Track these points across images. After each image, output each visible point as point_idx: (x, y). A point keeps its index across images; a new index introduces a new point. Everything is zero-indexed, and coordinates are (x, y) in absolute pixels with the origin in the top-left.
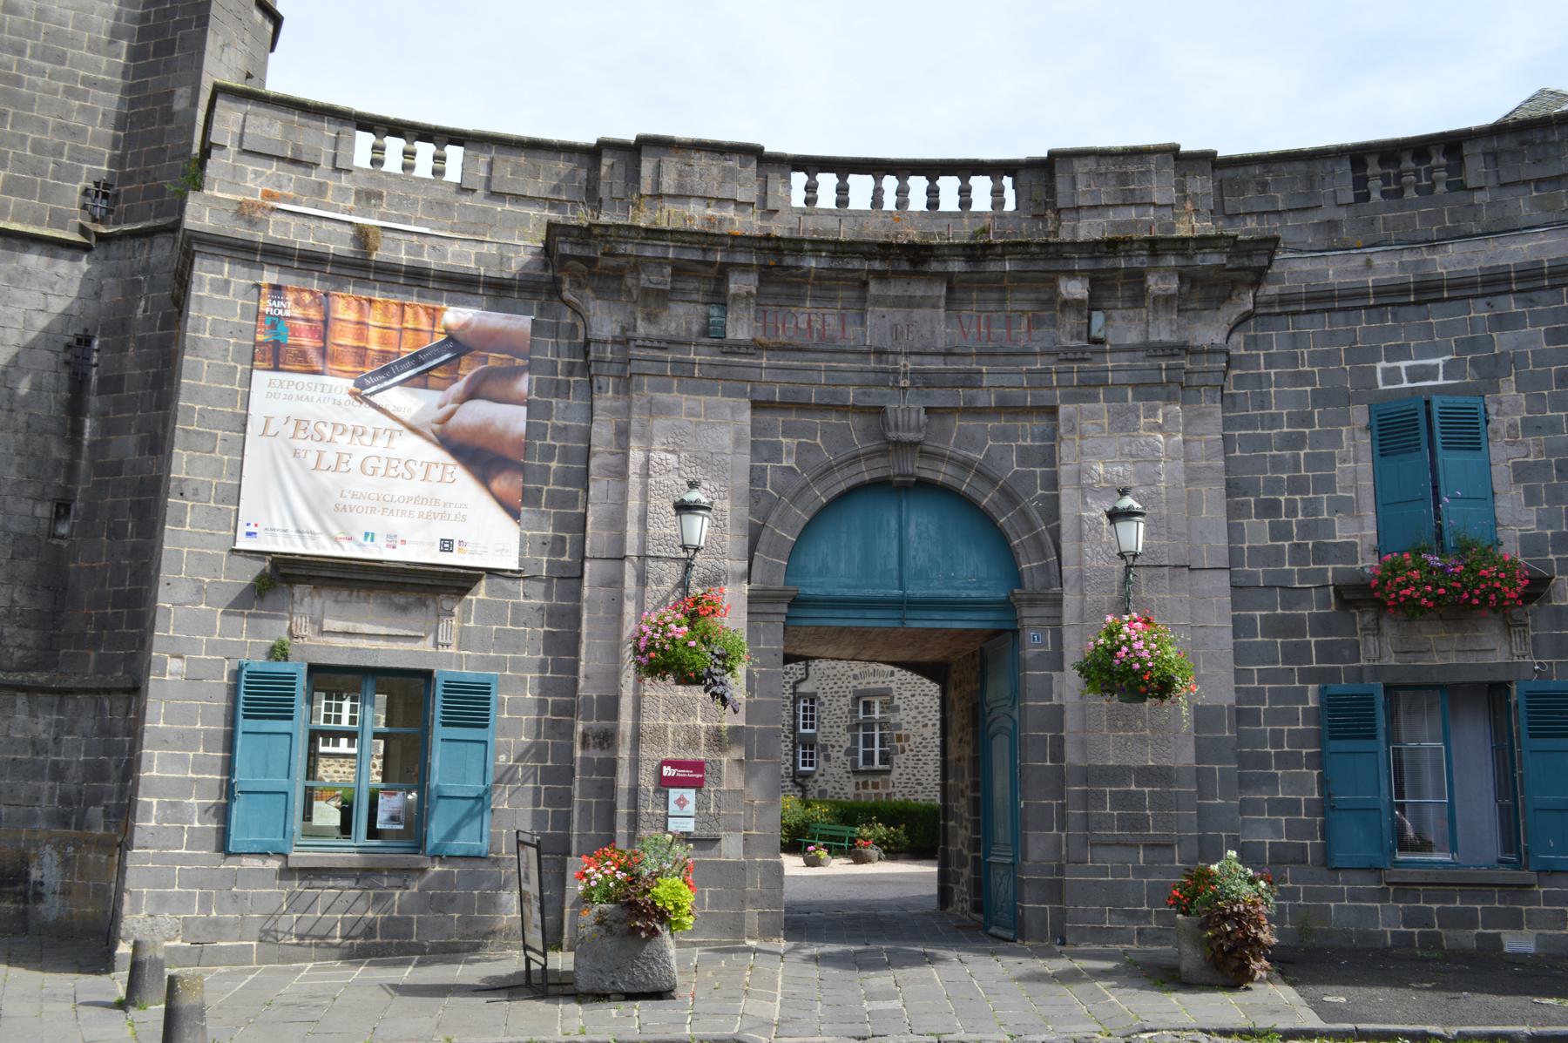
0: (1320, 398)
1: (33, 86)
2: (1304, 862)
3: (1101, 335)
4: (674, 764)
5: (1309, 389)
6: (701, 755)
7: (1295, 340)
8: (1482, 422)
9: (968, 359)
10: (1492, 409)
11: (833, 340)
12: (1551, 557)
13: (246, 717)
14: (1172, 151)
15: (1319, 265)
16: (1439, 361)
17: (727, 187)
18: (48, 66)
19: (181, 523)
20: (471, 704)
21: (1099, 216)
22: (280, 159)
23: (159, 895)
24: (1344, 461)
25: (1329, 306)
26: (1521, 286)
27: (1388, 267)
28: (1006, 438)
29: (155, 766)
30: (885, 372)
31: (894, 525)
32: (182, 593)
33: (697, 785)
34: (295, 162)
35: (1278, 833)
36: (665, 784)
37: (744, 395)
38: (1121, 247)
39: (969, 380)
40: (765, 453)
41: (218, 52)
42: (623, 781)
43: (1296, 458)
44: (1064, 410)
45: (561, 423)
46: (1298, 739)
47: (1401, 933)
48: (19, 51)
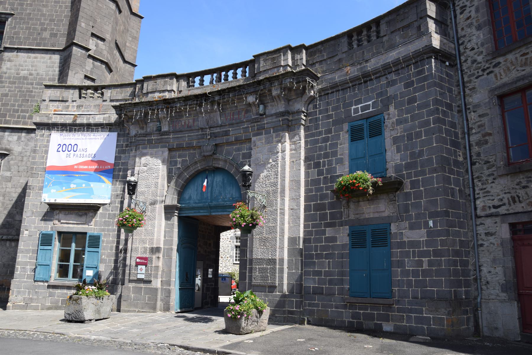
0: (335, 123)
1: (35, 92)
2: (323, 294)
6: (147, 255)
7: (328, 104)
8: (382, 122)
9: (226, 127)
10: (386, 117)
11: (191, 127)
12: (404, 172)
14: (289, 47)
15: (333, 76)
17: (165, 87)
18: (39, 87)
19: (29, 196)
20: (95, 241)
21: (266, 73)
22: (59, 101)
23: (18, 291)
24: (341, 145)
27: (351, 71)
29: (20, 258)
32: (29, 214)
33: (146, 265)
34: (62, 101)
35: (315, 283)
36: (137, 264)
37: (166, 147)
39: (227, 133)
40: (173, 164)
41: (73, 75)
43: (326, 146)
44: (253, 139)
47: (351, 322)
48: (32, 84)
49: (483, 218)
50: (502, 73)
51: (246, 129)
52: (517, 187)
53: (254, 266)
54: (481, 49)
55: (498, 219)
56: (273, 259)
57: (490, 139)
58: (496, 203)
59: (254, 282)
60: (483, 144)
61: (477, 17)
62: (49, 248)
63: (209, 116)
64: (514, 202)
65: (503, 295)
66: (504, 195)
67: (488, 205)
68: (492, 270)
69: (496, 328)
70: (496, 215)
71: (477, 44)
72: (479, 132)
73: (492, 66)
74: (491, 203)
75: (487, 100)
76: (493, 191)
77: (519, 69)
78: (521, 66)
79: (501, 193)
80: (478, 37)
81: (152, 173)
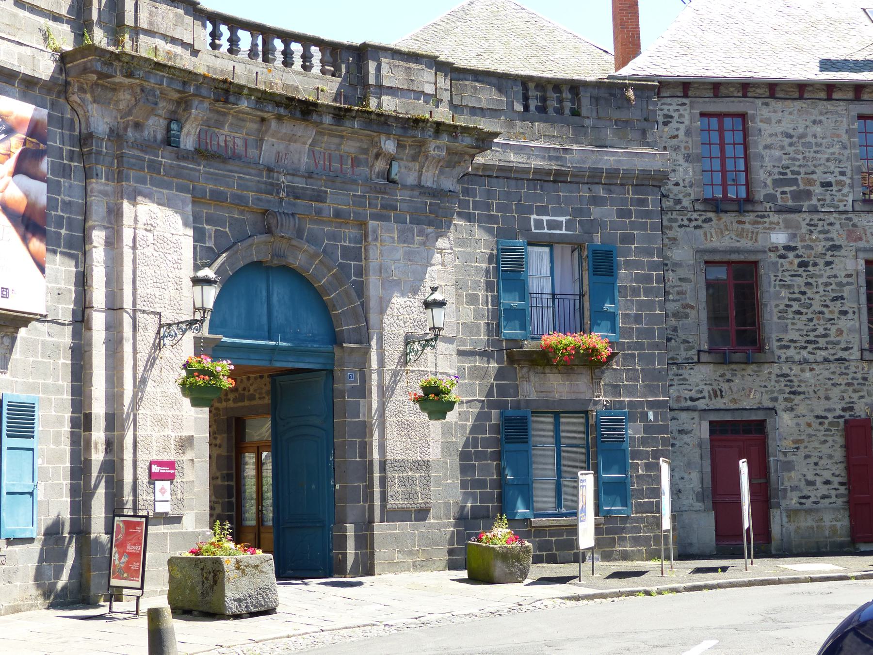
3: (397, 178)
4: (160, 464)
5: (495, 226)
6: (170, 456)
7: (489, 194)
13: (9, 436)
16: (563, 219)
25: (508, 175)
26: (607, 181)
28: (335, 239)
30: (272, 184)
31: (264, 293)
33: (171, 478)
36: (153, 478)
38: (421, 124)
42: (128, 478)
45: (67, 199)
46: (486, 443)
49: (676, 412)
50: (714, 235)
51: (359, 201)
52: (720, 379)
53: (389, 475)
54: (689, 190)
55: (696, 415)
56: (424, 462)
57: (692, 313)
58: (693, 394)
59: (391, 503)
60: (682, 317)
61: (687, 142)
62: (521, 446)
63: (287, 147)
64: (716, 396)
65: (699, 505)
66: (704, 387)
67: (683, 396)
68: (686, 476)
69: (691, 544)
70: (694, 409)
71: (684, 180)
72: (678, 301)
73: (701, 219)
74: (687, 394)
75: (692, 262)
76: (691, 380)
77: (734, 237)
78: (737, 236)
79: (700, 384)
80: (686, 172)
81: (160, 252)
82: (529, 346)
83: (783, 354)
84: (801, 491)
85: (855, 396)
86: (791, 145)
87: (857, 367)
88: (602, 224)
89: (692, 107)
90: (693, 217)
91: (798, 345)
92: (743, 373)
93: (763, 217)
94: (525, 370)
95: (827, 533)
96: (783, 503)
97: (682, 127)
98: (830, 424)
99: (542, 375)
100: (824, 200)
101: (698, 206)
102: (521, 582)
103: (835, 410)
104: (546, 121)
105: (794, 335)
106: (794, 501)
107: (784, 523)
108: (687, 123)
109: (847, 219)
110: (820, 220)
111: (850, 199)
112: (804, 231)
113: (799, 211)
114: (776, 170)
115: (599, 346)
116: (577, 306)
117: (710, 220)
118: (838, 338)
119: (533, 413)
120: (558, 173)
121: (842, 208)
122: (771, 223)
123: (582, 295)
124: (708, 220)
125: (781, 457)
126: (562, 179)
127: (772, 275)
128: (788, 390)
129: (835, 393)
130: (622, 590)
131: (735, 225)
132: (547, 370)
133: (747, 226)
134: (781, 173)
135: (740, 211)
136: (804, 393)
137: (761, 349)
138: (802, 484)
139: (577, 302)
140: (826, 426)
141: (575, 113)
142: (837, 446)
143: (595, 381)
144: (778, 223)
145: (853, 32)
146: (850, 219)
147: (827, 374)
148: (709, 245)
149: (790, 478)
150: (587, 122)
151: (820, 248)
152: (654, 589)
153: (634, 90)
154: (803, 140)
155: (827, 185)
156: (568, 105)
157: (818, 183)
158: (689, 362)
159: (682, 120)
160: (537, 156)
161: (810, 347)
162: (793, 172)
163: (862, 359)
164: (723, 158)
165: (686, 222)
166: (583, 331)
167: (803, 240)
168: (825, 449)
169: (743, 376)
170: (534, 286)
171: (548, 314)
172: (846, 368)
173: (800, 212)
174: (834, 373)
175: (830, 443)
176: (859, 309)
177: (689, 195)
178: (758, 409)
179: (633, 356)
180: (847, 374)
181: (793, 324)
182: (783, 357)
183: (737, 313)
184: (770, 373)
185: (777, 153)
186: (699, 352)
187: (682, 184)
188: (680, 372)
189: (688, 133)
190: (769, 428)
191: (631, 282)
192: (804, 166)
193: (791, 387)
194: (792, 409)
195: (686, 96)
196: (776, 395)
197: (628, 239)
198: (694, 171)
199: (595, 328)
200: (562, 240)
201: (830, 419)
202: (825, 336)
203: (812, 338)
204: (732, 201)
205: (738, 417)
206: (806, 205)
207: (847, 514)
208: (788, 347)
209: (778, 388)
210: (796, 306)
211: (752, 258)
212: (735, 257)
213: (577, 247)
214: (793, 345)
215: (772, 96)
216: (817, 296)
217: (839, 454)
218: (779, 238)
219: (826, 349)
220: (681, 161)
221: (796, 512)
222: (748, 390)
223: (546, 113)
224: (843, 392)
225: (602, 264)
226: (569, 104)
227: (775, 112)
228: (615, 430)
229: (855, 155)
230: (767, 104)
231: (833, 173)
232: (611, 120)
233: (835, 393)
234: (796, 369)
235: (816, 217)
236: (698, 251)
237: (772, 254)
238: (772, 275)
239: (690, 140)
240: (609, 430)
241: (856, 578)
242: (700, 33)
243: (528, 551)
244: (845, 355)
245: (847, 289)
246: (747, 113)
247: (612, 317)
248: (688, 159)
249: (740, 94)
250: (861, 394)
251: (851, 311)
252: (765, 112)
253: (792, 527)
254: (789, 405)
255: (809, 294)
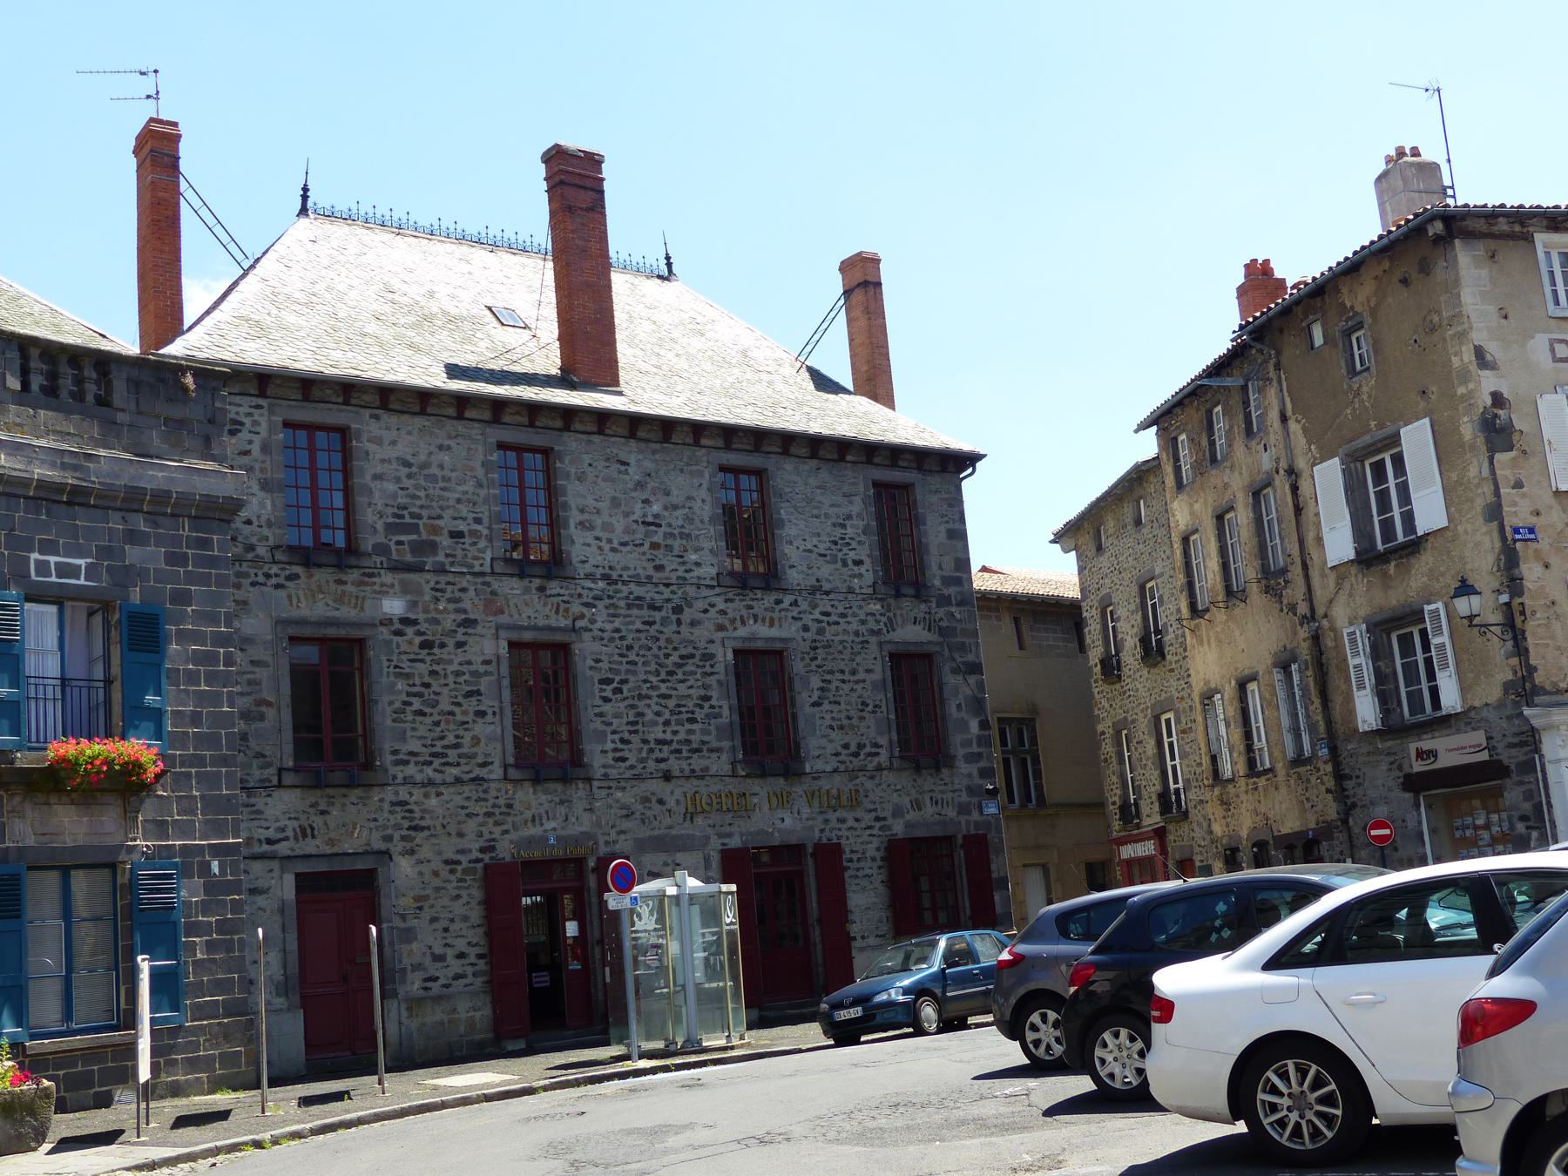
16: (82, 562)
54: (265, 531)
55: (275, 865)
57: (270, 713)
58: (271, 834)
64: (305, 836)
67: (256, 836)
74: (262, 834)
76: (270, 812)
80: (262, 505)
82: (23, 760)
83: (400, 772)
84: (425, 970)
85: (497, 830)
86: (409, 476)
87: (499, 790)
88: (142, 574)
89: (271, 412)
90: (272, 572)
91: (421, 759)
92: (343, 800)
93: (372, 575)
94: (17, 800)
95: (462, 1029)
96: (401, 991)
97: (257, 440)
98: (464, 871)
99: (45, 808)
100: (453, 556)
101: (279, 556)
102: (34, 1149)
103: (470, 851)
104: (57, 410)
105: (414, 745)
106: (416, 986)
107: (403, 1020)
108: (264, 434)
109: (484, 584)
110: (449, 583)
111: (488, 556)
112: (427, 598)
113: (418, 569)
114: (390, 511)
115: (143, 760)
116: (101, 697)
117: (296, 577)
118: (474, 750)
119: (30, 868)
120: (75, 490)
121: (477, 569)
122: (382, 585)
123: (108, 682)
124: (293, 577)
125: (398, 922)
126: (81, 500)
127: (384, 658)
128: (406, 824)
129: (471, 826)
130: (219, 1144)
131: (333, 586)
132: (53, 799)
133: (350, 588)
134: (395, 515)
135: (340, 566)
136: (428, 828)
137: (368, 765)
138: (428, 960)
139: (101, 692)
140: (459, 875)
141: (103, 402)
142: (474, 903)
143: (129, 815)
144: (393, 586)
145: (479, 335)
146: (487, 584)
147: (459, 800)
148: (295, 613)
149: (410, 953)
150: (120, 417)
151: (448, 624)
152: (267, 1136)
153: (194, 376)
154: (426, 472)
155: (457, 535)
156: (91, 389)
157: (445, 532)
158: (265, 786)
159: (258, 429)
160: (43, 462)
161: (437, 762)
162: (413, 515)
163: (505, 778)
164: (314, 489)
165: (261, 579)
166: (109, 734)
167: (426, 611)
168: (458, 908)
169: (343, 805)
170: (31, 666)
171: (54, 713)
172: (485, 791)
173: (422, 570)
174: (468, 798)
175: (465, 899)
176: (501, 709)
177: (267, 539)
178: (366, 853)
179: (188, 775)
180: (486, 800)
181: (413, 729)
182: (400, 776)
183: (329, 714)
184: (382, 800)
185: (391, 487)
186: (280, 770)
187: (256, 523)
188: (252, 800)
189: (265, 448)
190: (381, 879)
191: (186, 662)
192: (428, 507)
193: (412, 819)
194: (412, 852)
195: (262, 395)
196: (389, 831)
197: (182, 598)
198: (273, 505)
199: (131, 732)
200: (78, 594)
201: (465, 864)
202: (456, 746)
203: (438, 749)
204: (328, 551)
205: (337, 866)
206: (429, 562)
207: (488, 999)
208: (407, 763)
209: (392, 822)
210: (417, 704)
211: (356, 633)
212: (332, 632)
213: (99, 605)
214: (413, 759)
215: (384, 406)
216: (445, 691)
217: (476, 914)
218: (394, 606)
219: (458, 764)
220: (255, 488)
221: (420, 1001)
222: (351, 826)
223: (57, 397)
224: (481, 825)
225: (144, 634)
226: (93, 387)
227: (387, 428)
228: (159, 891)
229: (495, 496)
230: (377, 417)
231: (464, 519)
232: (157, 417)
233: (471, 826)
234: (418, 794)
235: (443, 579)
236: (281, 622)
237: (384, 629)
238: (384, 658)
239: (268, 458)
240: (151, 891)
241: (545, 1089)
242: (274, 311)
243: (48, 1096)
244: (483, 772)
245: (485, 680)
246: (349, 428)
247: (157, 715)
248: (265, 486)
249: (340, 400)
250: (505, 827)
251: (490, 711)
252: (374, 428)
253: (414, 1024)
254: (408, 846)
255: (435, 688)
